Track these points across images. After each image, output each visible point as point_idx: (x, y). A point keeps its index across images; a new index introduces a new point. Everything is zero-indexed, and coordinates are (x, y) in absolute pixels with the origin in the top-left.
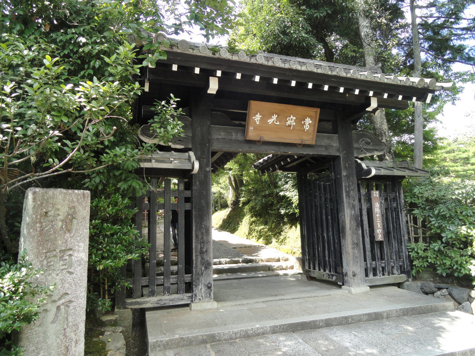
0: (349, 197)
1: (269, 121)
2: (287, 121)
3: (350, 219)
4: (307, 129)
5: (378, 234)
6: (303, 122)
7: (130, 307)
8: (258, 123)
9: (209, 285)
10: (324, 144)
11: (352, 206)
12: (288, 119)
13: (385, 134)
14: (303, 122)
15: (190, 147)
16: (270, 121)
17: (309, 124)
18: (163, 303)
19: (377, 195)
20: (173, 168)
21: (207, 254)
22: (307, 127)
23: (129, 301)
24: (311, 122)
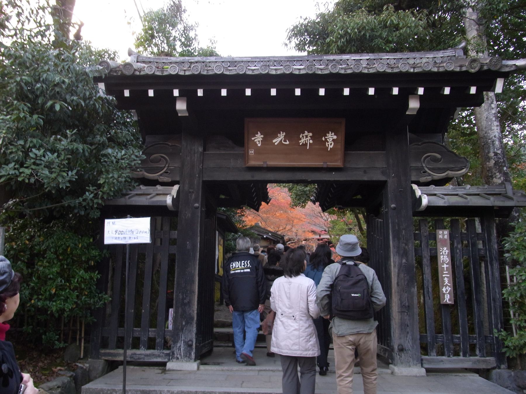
0: (399, 239)
1: (274, 141)
2: (301, 139)
3: (399, 270)
4: (331, 147)
5: (444, 294)
6: (323, 139)
7: (103, 358)
8: (259, 145)
9: (190, 343)
10: (361, 166)
11: (402, 252)
12: (301, 136)
13: (493, 145)
14: (323, 139)
15: (178, 179)
16: (276, 141)
17: (333, 140)
18: (137, 358)
19: (446, 237)
20: (147, 204)
21: (190, 306)
22: (330, 145)
23: (103, 351)
24: (335, 137)
